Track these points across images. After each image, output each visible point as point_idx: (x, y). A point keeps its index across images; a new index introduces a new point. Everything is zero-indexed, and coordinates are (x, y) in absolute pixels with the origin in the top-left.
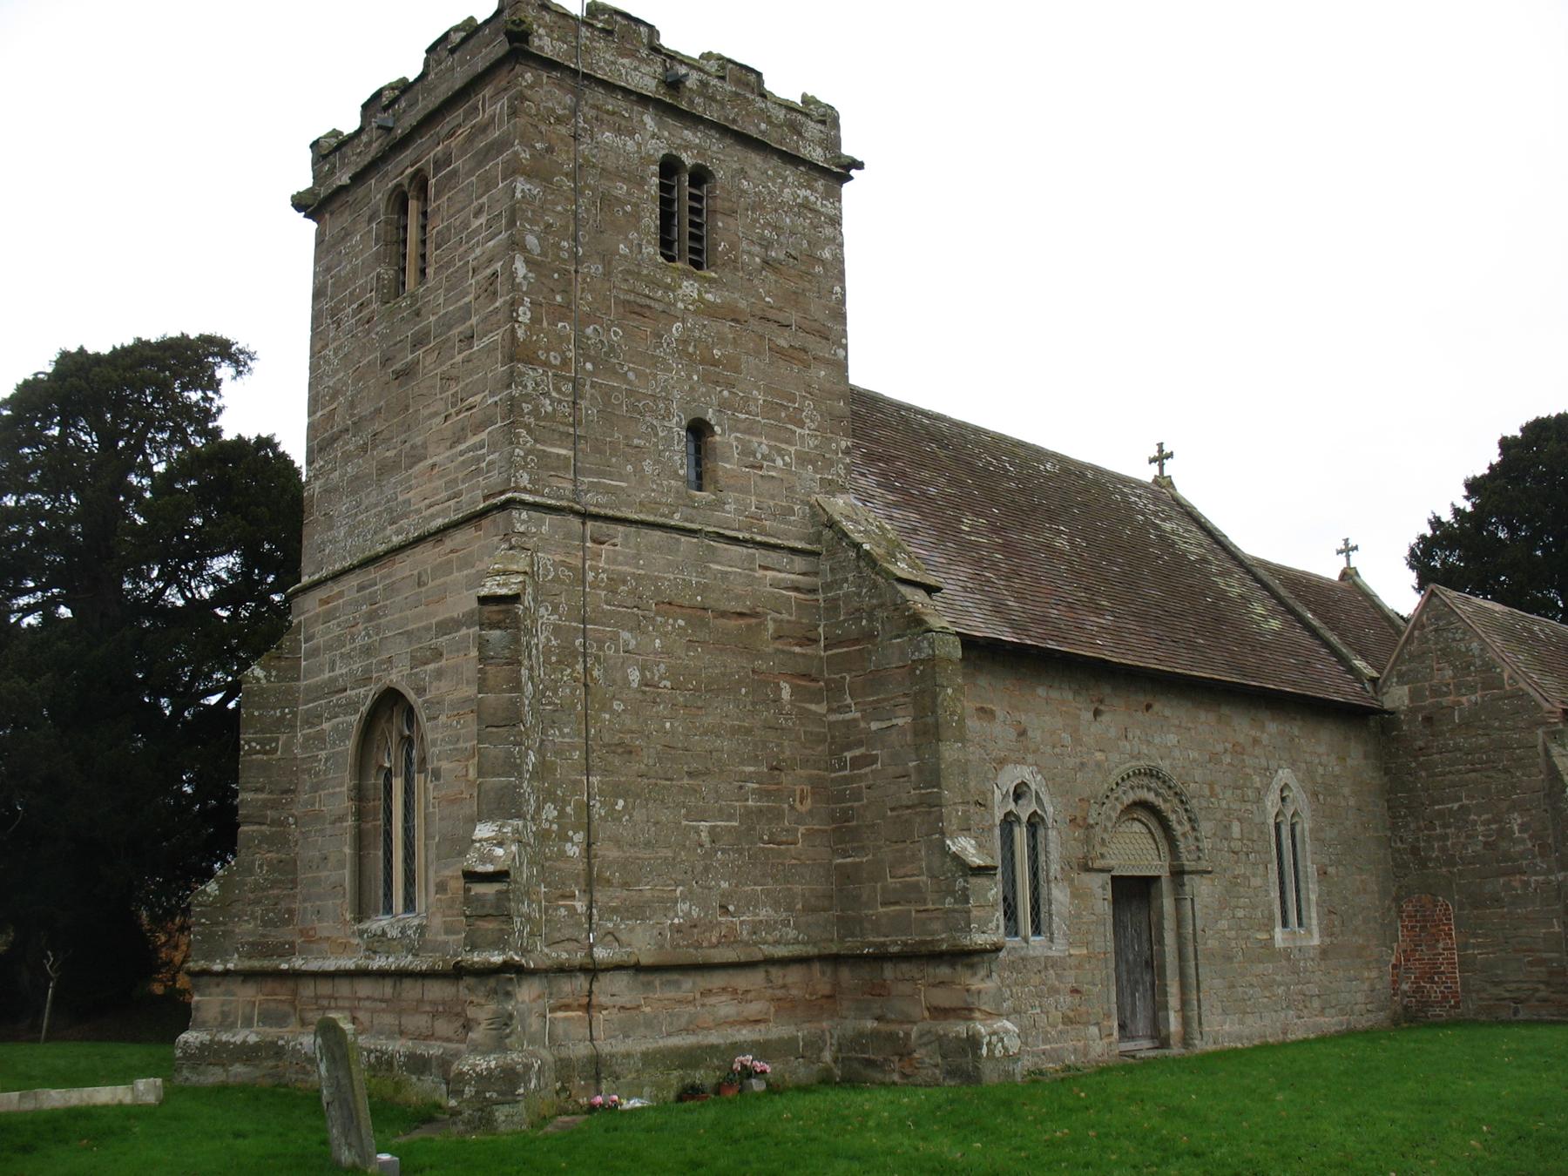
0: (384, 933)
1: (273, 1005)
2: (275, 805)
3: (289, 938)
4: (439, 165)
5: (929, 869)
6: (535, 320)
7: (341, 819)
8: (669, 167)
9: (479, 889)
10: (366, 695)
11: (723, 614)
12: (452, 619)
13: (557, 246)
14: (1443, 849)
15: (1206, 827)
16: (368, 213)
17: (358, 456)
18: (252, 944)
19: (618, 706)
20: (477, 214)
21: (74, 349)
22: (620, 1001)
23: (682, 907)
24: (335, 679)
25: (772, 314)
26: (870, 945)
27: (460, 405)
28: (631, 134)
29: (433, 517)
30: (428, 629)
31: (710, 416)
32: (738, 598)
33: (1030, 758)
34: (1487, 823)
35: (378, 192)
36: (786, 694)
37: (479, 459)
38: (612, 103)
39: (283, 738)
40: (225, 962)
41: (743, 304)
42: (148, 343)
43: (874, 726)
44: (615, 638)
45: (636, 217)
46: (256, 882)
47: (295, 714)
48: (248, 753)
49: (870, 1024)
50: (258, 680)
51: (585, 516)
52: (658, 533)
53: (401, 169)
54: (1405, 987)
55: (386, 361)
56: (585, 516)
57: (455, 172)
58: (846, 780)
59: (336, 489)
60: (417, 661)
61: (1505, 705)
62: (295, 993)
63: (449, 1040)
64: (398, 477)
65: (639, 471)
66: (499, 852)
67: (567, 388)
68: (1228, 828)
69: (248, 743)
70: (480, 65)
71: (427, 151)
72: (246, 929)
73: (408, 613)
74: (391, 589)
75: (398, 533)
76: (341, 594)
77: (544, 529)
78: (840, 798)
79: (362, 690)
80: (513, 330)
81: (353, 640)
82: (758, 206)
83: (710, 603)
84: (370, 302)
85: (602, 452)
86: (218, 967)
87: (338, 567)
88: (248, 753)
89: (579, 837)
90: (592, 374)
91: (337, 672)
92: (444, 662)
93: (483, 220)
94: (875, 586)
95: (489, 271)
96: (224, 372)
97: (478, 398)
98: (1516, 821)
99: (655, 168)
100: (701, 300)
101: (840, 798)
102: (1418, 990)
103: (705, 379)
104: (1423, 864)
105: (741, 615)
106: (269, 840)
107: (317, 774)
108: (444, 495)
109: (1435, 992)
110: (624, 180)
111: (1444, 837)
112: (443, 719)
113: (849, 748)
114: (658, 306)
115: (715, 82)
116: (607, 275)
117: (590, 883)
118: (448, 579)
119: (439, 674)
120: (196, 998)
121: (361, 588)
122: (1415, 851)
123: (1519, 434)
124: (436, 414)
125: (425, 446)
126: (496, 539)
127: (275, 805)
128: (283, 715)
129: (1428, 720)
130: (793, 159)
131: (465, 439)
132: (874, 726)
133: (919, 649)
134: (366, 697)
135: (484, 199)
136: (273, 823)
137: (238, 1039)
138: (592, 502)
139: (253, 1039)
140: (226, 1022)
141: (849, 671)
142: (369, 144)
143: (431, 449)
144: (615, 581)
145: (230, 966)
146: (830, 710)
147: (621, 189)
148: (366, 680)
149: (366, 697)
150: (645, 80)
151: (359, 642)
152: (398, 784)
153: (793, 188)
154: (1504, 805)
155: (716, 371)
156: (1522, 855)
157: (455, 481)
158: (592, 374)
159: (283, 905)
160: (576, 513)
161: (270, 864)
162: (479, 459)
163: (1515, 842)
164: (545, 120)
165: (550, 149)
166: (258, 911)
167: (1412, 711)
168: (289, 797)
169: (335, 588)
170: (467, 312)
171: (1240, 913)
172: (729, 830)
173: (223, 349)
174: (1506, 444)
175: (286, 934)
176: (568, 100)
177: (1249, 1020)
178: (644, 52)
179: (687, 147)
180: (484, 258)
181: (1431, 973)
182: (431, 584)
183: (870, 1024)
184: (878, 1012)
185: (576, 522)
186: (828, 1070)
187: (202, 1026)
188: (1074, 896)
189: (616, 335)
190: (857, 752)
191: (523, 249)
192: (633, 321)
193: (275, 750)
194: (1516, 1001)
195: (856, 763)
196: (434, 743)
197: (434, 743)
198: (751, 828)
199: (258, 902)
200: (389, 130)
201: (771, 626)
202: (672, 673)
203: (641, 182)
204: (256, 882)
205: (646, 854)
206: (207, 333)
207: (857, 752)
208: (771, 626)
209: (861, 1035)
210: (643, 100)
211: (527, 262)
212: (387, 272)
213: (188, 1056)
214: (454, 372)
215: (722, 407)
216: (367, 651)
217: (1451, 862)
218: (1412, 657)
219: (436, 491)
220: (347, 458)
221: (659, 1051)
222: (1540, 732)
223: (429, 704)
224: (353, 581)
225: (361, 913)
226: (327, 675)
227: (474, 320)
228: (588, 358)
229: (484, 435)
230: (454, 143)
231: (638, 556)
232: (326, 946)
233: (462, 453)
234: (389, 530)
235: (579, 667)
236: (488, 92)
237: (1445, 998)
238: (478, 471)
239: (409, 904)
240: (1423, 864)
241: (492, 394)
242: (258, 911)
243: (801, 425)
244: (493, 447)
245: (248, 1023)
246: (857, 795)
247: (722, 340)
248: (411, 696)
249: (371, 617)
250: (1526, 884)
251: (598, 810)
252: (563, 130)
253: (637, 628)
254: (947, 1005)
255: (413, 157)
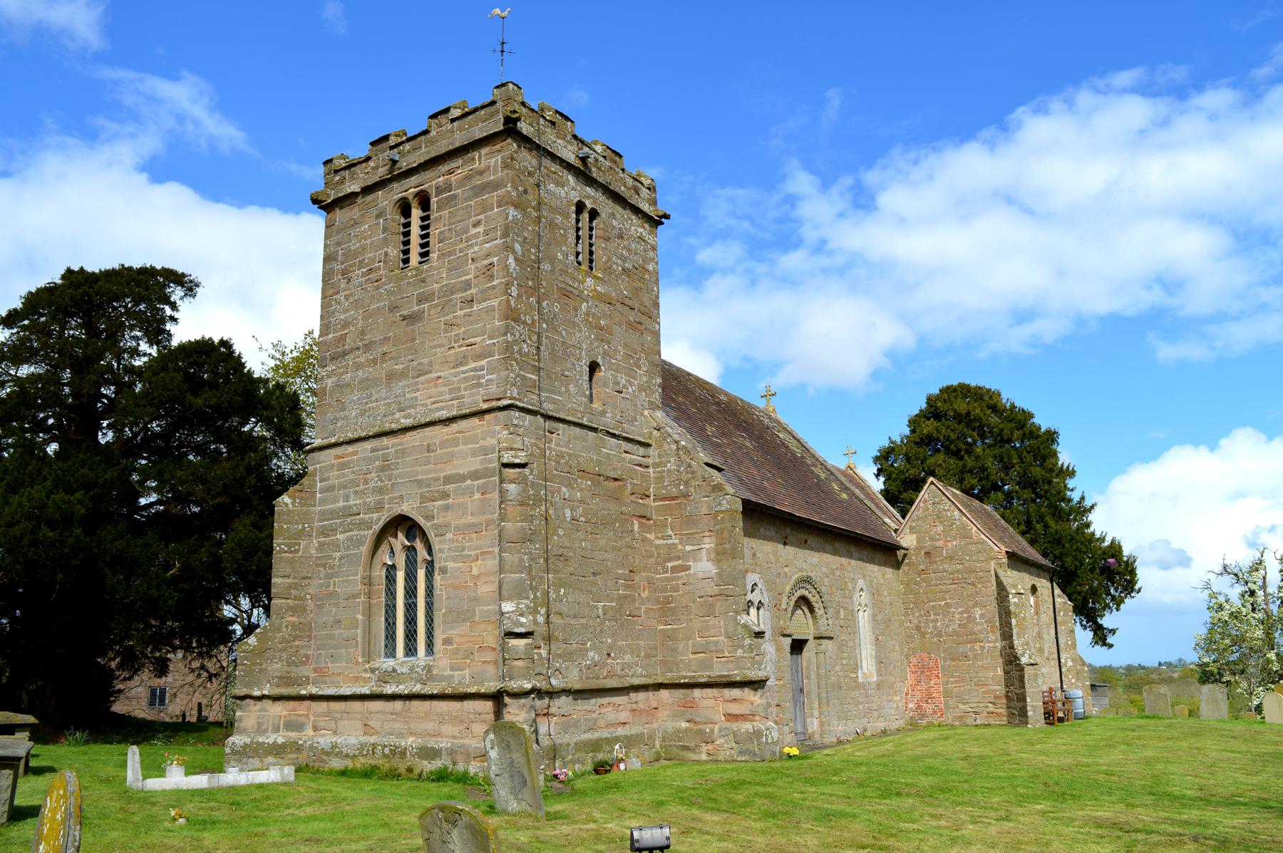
0: (394, 670)
1: (294, 718)
2: (296, 586)
3: (306, 673)
4: (439, 191)
5: (726, 632)
6: (519, 296)
7: (355, 596)
8: (580, 207)
9: (514, 642)
10: (382, 518)
11: (608, 478)
12: (459, 475)
13: (528, 250)
14: (935, 627)
15: (831, 611)
16: (375, 212)
17: (369, 366)
18: (280, 678)
19: (561, 532)
20: (476, 225)
21: (76, 268)
22: (563, 711)
23: (591, 654)
24: (350, 507)
25: (627, 302)
26: (685, 677)
27: (461, 342)
28: (563, 186)
29: (438, 409)
30: (437, 479)
31: (599, 360)
32: (615, 469)
33: (758, 569)
34: (962, 613)
35: (386, 199)
36: (636, 528)
37: (479, 377)
38: (555, 167)
39: (303, 543)
40: (261, 689)
41: (614, 294)
42: (130, 269)
43: (688, 548)
44: (559, 491)
45: (565, 236)
46: (283, 637)
47: (312, 528)
48: (279, 552)
49: (684, 725)
50: (287, 505)
51: (547, 417)
52: (577, 430)
53: (408, 188)
54: (911, 705)
55: (393, 308)
56: (547, 417)
57: (455, 197)
58: (667, 579)
59: (348, 385)
60: (424, 499)
61: (973, 548)
62: (309, 709)
63: (454, 737)
64: (406, 382)
65: (568, 391)
66: (523, 620)
67: (535, 338)
68: (838, 612)
69: (279, 545)
70: (478, 134)
71: (432, 181)
72: (276, 667)
73: (419, 468)
74: (403, 452)
75: (406, 417)
76: (355, 453)
77: (526, 423)
78: (664, 590)
79: (375, 515)
80: (508, 300)
81: (366, 482)
82: (621, 237)
83: (602, 472)
84: (379, 268)
85: (551, 378)
86: (257, 693)
87: (350, 435)
88: (279, 552)
89: (543, 611)
90: (546, 331)
91: (351, 502)
92: (451, 501)
93: (481, 229)
94: (690, 466)
95: (486, 262)
96: (177, 293)
97: (478, 339)
98: (978, 612)
99: (574, 208)
100: (595, 290)
101: (664, 590)
102: (919, 707)
103: (597, 338)
104: (923, 635)
105: (616, 479)
106: (293, 610)
107: (332, 567)
108: (448, 397)
109: (929, 708)
110: (560, 214)
111: (936, 621)
112: (449, 536)
113: (670, 560)
114: (576, 292)
115: (601, 159)
116: (552, 271)
117: (548, 639)
118: (455, 449)
119: (447, 508)
120: (238, 714)
121: (373, 450)
122: (918, 628)
123: (59, 282)
124: (440, 346)
125: (430, 364)
126: (498, 428)
127: (296, 586)
128: (304, 528)
129: (927, 553)
130: (636, 210)
131: (467, 364)
132: (688, 548)
133: (720, 504)
134: (379, 520)
135: (482, 217)
136: (295, 598)
137: (271, 741)
138: (548, 408)
139: (280, 740)
140: (260, 730)
141: (671, 515)
142: (377, 168)
143: (436, 367)
144: (560, 455)
145: (266, 692)
146: (657, 538)
147: (559, 219)
148: (379, 507)
149: (379, 520)
150: (569, 153)
151: (372, 485)
152: (400, 576)
153: (637, 228)
154: (971, 604)
155: (602, 334)
156: (980, 632)
157: (459, 389)
158: (546, 331)
159: (302, 652)
160: (542, 415)
161: (293, 625)
162: (479, 377)
163: (978, 624)
164: (523, 173)
165: (526, 192)
166: (285, 656)
167: (918, 549)
168: (307, 581)
169: (350, 449)
170: (467, 285)
171: (844, 662)
172: (612, 608)
173: (177, 278)
174: (930, 400)
175: (306, 671)
176: (534, 162)
177: (850, 723)
178: (569, 137)
179: (588, 197)
180: (482, 253)
181: (928, 697)
182: (439, 451)
183: (684, 725)
184: (689, 717)
185: (540, 419)
186: (658, 753)
187: (244, 731)
188: (777, 650)
189: (557, 308)
190: (676, 563)
191: (514, 252)
192: (567, 300)
193: (298, 551)
194: (976, 713)
195: (674, 569)
196: (441, 551)
197: (441, 551)
198: (621, 607)
199: (284, 650)
200: (394, 162)
201: (629, 487)
202: (585, 514)
203: (568, 217)
204: (283, 637)
205: (574, 622)
206: (167, 266)
207: (676, 563)
208: (629, 487)
209: (679, 731)
210: (569, 166)
211: (516, 259)
212: (394, 252)
213: (234, 753)
214: (457, 321)
215: (605, 354)
216: (380, 490)
217: (939, 634)
218: (919, 518)
219: (441, 394)
220: (358, 366)
221: (581, 742)
222: (992, 563)
223: (437, 527)
224: (368, 445)
225: (369, 657)
226: (341, 504)
227: (474, 291)
228: (545, 321)
229: (484, 362)
230: (453, 178)
231: (569, 442)
232: (339, 679)
233: (464, 372)
234: (397, 415)
235: (543, 508)
236: (484, 151)
237: (935, 712)
238: (479, 385)
239: (411, 650)
240: (923, 635)
241: (490, 338)
242: (285, 656)
243: (640, 368)
244: (491, 370)
245: (276, 730)
246: (676, 589)
247: (604, 316)
248: (421, 521)
249: (382, 469)
250: (983, 648)
251: (553, 595)
252: (531, 180)
253: (569, 486)
254: (738, 712)
255: (417, 182)
